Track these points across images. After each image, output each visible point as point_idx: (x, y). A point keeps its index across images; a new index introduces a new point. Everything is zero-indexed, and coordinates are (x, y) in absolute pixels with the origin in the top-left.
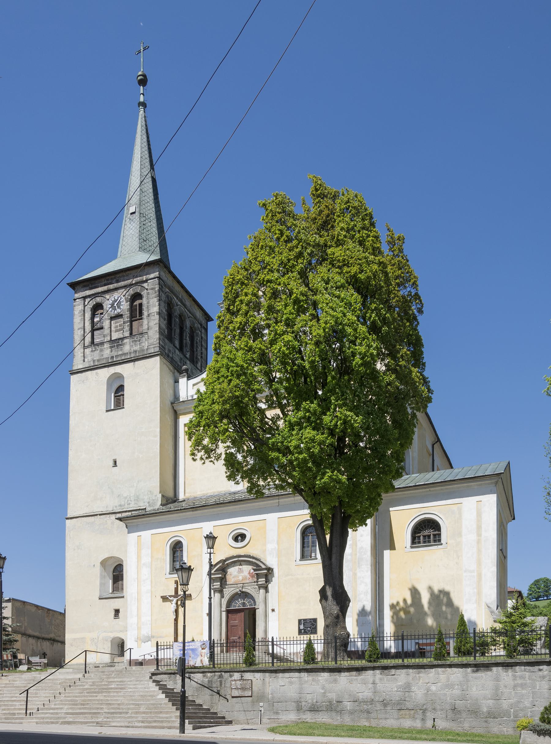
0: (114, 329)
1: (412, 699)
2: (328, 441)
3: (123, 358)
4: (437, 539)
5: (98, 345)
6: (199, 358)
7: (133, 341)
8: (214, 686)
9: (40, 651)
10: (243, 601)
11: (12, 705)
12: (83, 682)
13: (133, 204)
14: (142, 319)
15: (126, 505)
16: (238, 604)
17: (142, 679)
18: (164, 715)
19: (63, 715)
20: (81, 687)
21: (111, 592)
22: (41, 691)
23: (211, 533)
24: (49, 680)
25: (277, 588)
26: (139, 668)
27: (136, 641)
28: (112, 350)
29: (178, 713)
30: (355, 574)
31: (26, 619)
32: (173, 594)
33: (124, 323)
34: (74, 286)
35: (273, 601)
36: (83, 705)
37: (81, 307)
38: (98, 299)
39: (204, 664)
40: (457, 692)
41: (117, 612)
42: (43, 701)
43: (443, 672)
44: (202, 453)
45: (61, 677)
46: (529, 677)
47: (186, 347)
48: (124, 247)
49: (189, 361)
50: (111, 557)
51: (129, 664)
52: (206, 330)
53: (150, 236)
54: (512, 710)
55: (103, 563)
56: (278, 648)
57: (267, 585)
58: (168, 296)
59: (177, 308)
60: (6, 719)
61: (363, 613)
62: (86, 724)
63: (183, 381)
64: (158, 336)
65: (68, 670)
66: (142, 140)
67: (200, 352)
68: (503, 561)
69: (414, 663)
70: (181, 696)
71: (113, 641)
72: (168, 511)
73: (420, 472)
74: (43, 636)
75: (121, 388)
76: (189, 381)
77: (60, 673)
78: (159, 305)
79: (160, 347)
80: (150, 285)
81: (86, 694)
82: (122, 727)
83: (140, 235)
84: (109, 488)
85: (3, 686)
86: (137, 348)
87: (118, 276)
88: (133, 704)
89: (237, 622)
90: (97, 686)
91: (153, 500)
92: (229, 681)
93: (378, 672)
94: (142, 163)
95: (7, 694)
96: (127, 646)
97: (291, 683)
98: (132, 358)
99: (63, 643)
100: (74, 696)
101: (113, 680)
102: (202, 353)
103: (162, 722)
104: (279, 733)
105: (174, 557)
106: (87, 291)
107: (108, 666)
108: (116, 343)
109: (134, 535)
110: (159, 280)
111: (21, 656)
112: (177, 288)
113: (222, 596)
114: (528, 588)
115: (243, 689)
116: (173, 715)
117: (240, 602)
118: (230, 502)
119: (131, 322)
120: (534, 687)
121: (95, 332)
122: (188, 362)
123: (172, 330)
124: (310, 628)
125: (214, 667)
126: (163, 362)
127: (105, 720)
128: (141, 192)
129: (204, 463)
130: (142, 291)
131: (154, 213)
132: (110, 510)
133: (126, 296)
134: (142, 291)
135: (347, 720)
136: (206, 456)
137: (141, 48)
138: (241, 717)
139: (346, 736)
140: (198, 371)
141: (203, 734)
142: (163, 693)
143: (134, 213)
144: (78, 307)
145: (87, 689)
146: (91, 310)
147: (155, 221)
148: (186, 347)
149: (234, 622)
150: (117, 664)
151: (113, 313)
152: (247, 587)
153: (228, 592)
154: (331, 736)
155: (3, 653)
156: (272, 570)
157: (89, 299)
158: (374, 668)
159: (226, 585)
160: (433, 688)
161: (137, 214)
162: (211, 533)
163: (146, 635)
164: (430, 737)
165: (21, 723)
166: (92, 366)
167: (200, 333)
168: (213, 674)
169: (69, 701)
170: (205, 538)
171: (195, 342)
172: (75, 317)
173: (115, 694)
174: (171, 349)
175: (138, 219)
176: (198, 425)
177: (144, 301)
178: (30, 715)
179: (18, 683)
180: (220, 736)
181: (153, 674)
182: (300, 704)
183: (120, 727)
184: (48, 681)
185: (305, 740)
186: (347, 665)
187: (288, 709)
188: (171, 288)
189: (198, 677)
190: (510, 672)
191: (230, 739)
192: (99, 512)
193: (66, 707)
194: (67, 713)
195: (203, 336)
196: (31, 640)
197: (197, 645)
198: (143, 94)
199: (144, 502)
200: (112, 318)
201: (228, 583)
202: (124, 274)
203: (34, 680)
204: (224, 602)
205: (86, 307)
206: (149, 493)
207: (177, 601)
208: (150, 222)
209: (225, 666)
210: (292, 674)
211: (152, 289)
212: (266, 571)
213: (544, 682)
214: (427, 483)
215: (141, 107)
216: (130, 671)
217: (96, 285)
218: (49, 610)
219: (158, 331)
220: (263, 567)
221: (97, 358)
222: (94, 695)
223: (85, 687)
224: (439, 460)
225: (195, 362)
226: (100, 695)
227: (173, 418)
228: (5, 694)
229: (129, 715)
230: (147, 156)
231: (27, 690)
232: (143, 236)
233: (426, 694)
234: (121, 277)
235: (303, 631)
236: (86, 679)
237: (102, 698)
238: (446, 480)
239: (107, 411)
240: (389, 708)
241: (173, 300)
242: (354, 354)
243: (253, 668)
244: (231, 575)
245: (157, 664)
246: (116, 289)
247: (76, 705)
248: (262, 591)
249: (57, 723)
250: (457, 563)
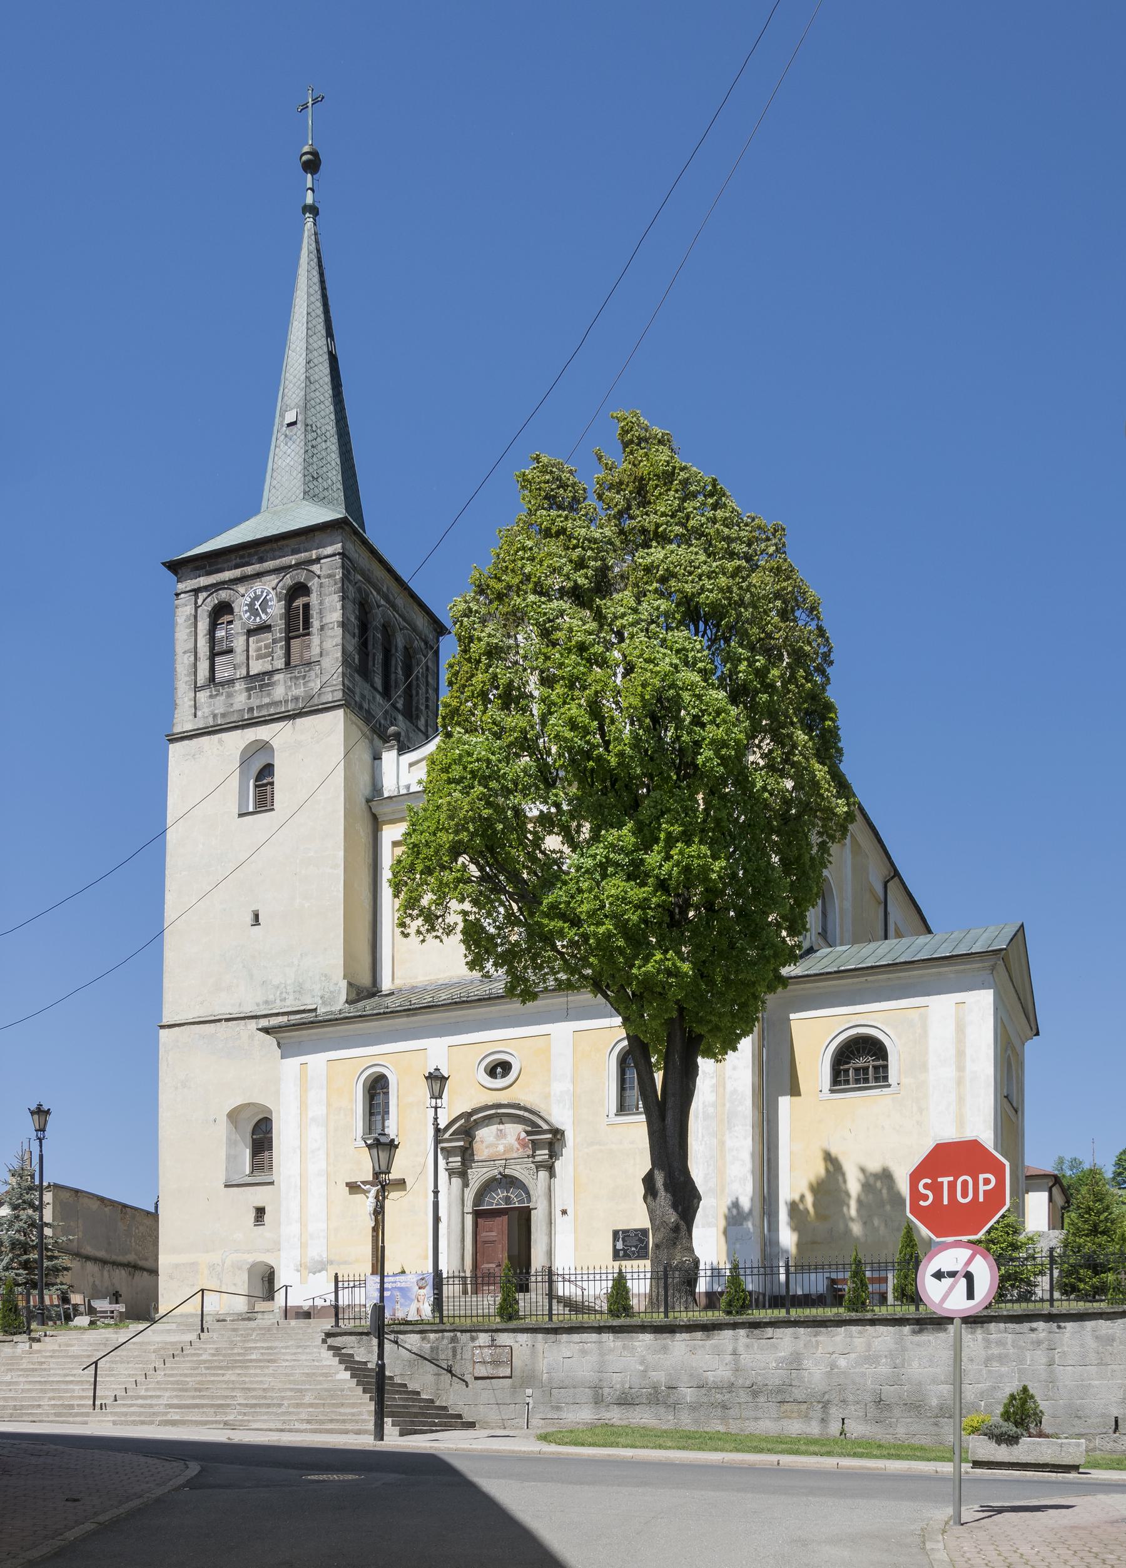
0: (254, 654)
1: (803, 1382)
2: (654, 900)
3: (272, 711)
4: (881, 1076)
5: (222, 684)
6: (423, 708)
7: (291, 678)
8: (442, 1357)
9: (107, 1288)
10: (505, 1194)
11: (66, 1391)
12: (198, 1349)
13: (292, 405)
14: (308, 634)
15: (278, 1001)
16: (496, 1200)
17: (308, 1343)
18: (348, 1410)
19: (162, 1409)
20: (195, 1359)
21: (247, 1172)
22: (119, 1365)
23: (437, 1069)
24: (134, 1343)
25: (571, 1168)
26: (302, 1323)
27: (298, 1271)
29: (372, 1407)
30: (722, 1143)
31: (80, 1225)
32: (371, 1178)
33: (274, 641)
34: (176, 567)
35: (563, 1194)
36: (200, 1390)
37: (189, 610)
38: (224, 595)
39: (424, 1317)
40: (884, 1369)
41: (260, 1212)
42: (124, 1383)
43: (860, 1332)
44: (420, 921)
45: (157, 1338)
46: (1013, 1342)
47: (396, 687)
48: (273, 491)
49: (403, 715)
51: (283, 1315)
52: (437, 653)
53: (324, 469)
55: (234, 1116)
56: (573, 1287)
57: (553, 1163)
58: (359, 590)
59: (378, 612)
60: (56, 1415)
61: (735, 1217)
62: (206, 1424)
63: (389, 757)
65: (167, 1327)
66: (309, 279)
67: (424, 696)
68: (1014, 1119)
69: (807, 1316)
70: (378, 1374)
71: (252, 1269)
72: (360, 1016)
73: (857, 939)
74: (114, 1257)
75: (268, 770)
76: (401, 758)
77: (154, 1332)
78: (343, 608)
79: (344, 691)
81: (204, 1371)
82: (270, 1430)
83: (305, 468)
84: (244, 967)
85: (48, 1354)
86: (299, 691)
87: (263, 548)
88: (291, 1390)
89: (494, 1234)
90: (224, 1355)
91: (331, 992)
92: (470, 1349)
93: (742, 1332)
94: (310, 325)
95: (55, 1369)
96: (281, 1280)
97: (584, 1352)
98: (288, 711)
99: (154, 1272)
100: (181, 1375)
101: (254, 1345)
102: (427, 699)
103: (344, 1421)
104: (556, 1443)
105: (371, 1106)
106: (202, 579)
107: (243, 1319)
108: (259, 681)
109: (294, 1062)
111: (76, 1299)
112: (379, 573)
113: (466, 1184)
114: (1114, 1160)
115: (496, 1363)
116: (364, 1409)
117: (501, 1196)
118: (479, 1000)
119: (288, 640)
120: (1021, 1360)
121: (218, 659)
122: (400, 717)
123: (367, 655)
124: (636, 1247)
125: (442, 1322)
126: (351, 720)
127: (240, 1417)
128: (308, 383)
129: (423, 941)
130: (310, 581)
131: (333, 424)
132: (249, 1009)
133: (278, 590)
135: (686, 1421)
136: (426, 927)
137: (307, 99)
138: (493, 1415)
139: (674, 1448)
140: (420, 733)
141: (419, 1443)
142: (346, 1369)
143: (293, 424)
144: (184, 610)
145: (205, 1361)
146: (210, 616)
147: (335, 440)
148: (396, 687)
149: (488, 1234)
150: (259, 1316)
153: (478, 1175)
154: (647, 1447)
155: (45, 1291)
157: (205, 594)
158: (735, 1326)
159: (473, 1161)
160: (842, 1362)
161: (299, 425)
162: (437, 1069)
163: (317, 1258)
164: (824, 1449)
165: (86, 1423)
166: (212, 727)
169: (172, 1383)
170: (427, 1078)
172: (178, 629)
173: (258, 1371)
174: (366, 693)
175: (302, 437)
176: (412, 869)
177: (314, 599)
178: (101, 1409)
179: (75, 1350)
180: (446, 1446)
181: (329, 1335)
182: (600, 1391)
183: (266, 1430)
184: (132, 1346)
185: (594, 1452)
186: (685, 1319)
187: (578, 1401)
188: (367, 572)
189: (412, 1340)
190: (980, 1332)
191: (463, 1449)
192: (224, 1014)
193: (167, 1394)
194: (171, 1406)
195: (430, 664)
196: (89, 1265)
197: (410, 1280)
198: (312, 189)
199: (313, 997)
200: (250, 633)
201: (476, 1158)
202: (275, 545)
203: (105, 1345)
204: (470, 1194)
205: (199, 610)
206: (323, 978)
208: (326, 441)
209: (463, 1319)
210: (585, 1336)
211: (329, 576)
212: (549, 1136)
213: (1039, 1352)
214: (860, 966)
215: (308, 215)
216: (285, 1328)
217: (219, 566)
218: (125, 1206)
220: (545, 1127)
221: (222, 711)
222: (220, 1372)
223: (201, 1358)
224: (898, 912)
225: (414, 717)
226: (230, 1372)
227: (369, 830)
228: (53, 1369)
229: (283, 1409)
230: (320, 311)
231: (96, 1363)
232: (311, 470)
233: (829, 1374)
234: (268, 552)
235: (621, 1253)
236: (204, 1343)
237: (233, 1378)
238: (898, 961)
239: (241, 815)
240: (762, 1399)
242: (697, 744)
243: (513, 1324)
244: (482, 1142)
245: (337, 1315)
246: (259, 575)
247: (186, 1390)
248: (543, 1175)
249: (152, 1423)
250: (918, 1122)
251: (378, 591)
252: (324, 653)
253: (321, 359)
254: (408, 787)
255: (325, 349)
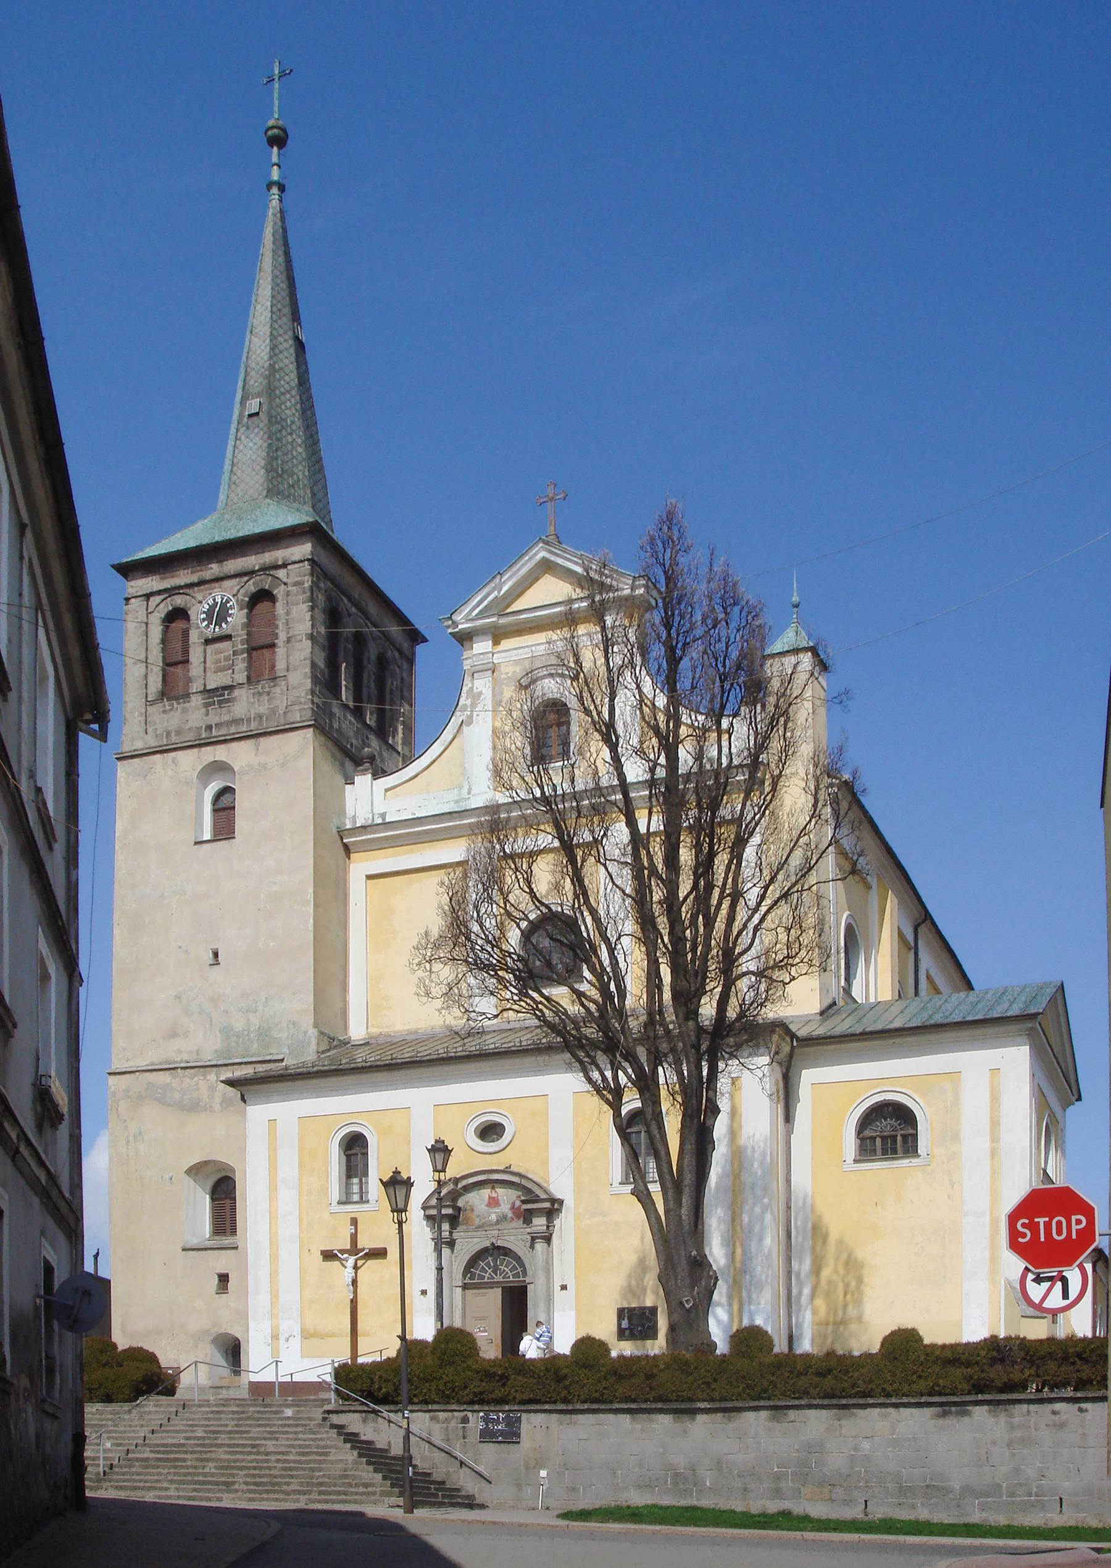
3: (233, 730)
21: (208, 1236)
28: (208, 710)
32: (348, 1247)
33: (235, 653)
38: (179, 601)
41: (224, 1279)
50: (206, 1162)
52: (411, 661)
53: (290, 464)
54: (1004, 1485)
64: (309, 686)
72: (336, 1070)
78: (312, 618)
80: (292, 574)
86: (262, 709)
94: (275, 309)
108: (219, 695)
110: (312, 566)
132: (208, 1057)
133: (240, 596)
134: (272, 585)
151: (213, 630)
152: (506, 1238)
156: (561, 1202)
157: (158, 599)
167: (398, 670)
168: (450, 1413)
171: (388, 690)
198: (282, 188)
200: (208, 642)
206: (291, 1026)
207: (356, 1260)
211: (297, 584)
219: (309, 674)
220: (543, 1196)
241: (341, 604)
246: (218, 580)
248: (540, 1246)
250: (949, 1196)
251: (350, 599)
252: (291, 667)
253: (286, 345)
254: (383, 815)
255: (290, 333)
